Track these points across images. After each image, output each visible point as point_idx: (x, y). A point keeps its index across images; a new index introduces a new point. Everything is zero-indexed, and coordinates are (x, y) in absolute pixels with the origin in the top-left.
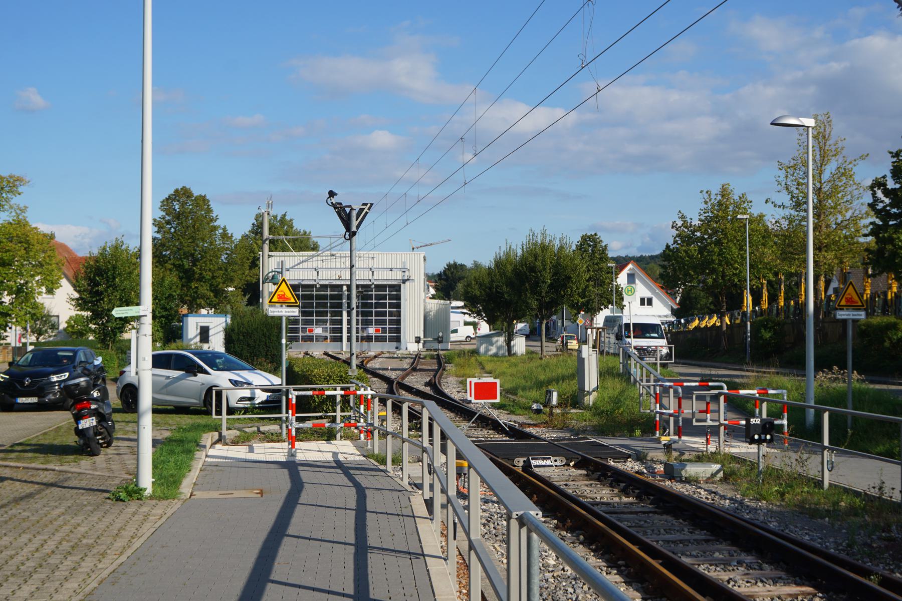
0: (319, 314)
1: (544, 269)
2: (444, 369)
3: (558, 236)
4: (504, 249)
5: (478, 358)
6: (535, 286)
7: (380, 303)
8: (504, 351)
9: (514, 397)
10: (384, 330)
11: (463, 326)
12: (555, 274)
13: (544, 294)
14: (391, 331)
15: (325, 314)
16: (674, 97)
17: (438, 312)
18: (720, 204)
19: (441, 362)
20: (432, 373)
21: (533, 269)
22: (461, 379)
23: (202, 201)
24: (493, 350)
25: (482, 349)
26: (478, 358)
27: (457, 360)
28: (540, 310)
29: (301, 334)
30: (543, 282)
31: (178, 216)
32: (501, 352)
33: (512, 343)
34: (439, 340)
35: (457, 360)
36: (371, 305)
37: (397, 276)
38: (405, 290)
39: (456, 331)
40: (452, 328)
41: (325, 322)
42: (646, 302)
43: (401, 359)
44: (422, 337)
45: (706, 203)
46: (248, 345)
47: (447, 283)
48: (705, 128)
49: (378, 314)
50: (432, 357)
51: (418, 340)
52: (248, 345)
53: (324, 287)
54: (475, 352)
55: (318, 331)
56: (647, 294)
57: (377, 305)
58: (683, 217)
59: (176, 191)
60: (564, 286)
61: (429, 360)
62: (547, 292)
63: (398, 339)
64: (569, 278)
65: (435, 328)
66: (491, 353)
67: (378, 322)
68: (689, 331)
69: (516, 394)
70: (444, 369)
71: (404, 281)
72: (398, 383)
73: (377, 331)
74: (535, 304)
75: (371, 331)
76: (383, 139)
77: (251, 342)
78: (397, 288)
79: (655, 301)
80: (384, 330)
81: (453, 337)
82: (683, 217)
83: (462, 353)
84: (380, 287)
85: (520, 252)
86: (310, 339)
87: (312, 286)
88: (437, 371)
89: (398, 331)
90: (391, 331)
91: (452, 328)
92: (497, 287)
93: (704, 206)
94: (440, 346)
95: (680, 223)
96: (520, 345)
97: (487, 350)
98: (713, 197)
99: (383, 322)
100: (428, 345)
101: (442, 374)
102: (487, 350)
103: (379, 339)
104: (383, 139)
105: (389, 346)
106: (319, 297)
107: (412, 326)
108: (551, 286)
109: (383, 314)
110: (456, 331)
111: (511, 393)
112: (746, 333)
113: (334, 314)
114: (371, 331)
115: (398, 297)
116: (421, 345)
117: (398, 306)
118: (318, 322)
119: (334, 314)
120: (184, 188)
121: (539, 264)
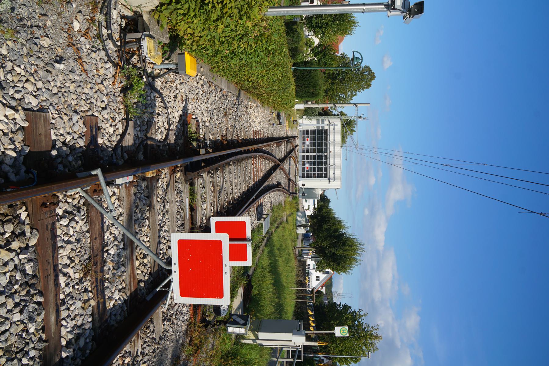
0: (315, 143)
1: (344, 251)
2: (289, 195)
3: (361, 258)
4: (346, 224)
5: (295, 212)
6: (333, 245)
7: (319, 167)
8: (299, 224)
9: (264, 243)
10: (307, 171)
11: (309, 206)
12: (341, 256)
13: (329, 249)
14: (307, 174)
15: (315, 146)
16: (389, 285)
17: (315, 194)
18: (371, 335)
19: (294, 194)
20: (287, 188)
21: (344, 244)
22: (283, 204)
23: (369, 86)
24: (299, 219)
25: (300, 214)
26: (295, 212)
27: (294, 202)
28: (321, 247)
29: (306, 136)
30: (337, 250)
31: (362, 73)
32: (298, 223)
33: (302, 228)
34: (303, 194)
35: (294, 202)
36: (318, 165)
37: (331, 177)
38: (325, 180)
39: (306, 201)
40: (308, 200)
41: (311, 146)
42: (318, 278)
43: (295, 176)
44: (305, 187)
45: (372, 327)
46: (303, 74)
47: (324, 200)
48: (377, 296)
49: (314, 168)
50: (296, 191)
51: (303, 185)
52: (303, 74)
53: (326, 144)
54: (298, 210)
55: (307, 143)
56: (321, 279)
57: (318, 168)
58: (365, 315)
59: (374, 73)
60: (334, 261)
61: (294, 189)
62: (331, 251)
63: (304, 177)
64: (339, 264)
65: (308, 193)
66: (298, 218)
67: (311, 168)
68: (307, 310)
69: (266, 245)
70: (289, 195)
71: (329, 179)
72: (279, 165)
73: (307, 168)
74: (324, 244)
75: (307, 165)
76: (372, 181)
77: (305, 75)
78: (326, 176)
79: (318, 282)
80: (307, 171)
81: (304, 200)
82: (365, 315)
83: (297, 204)
84: (326, 169)
85: (344, 231)
86: (304, 139)
87: (326, 140)
88: (289, 191)
89: (307, 177)
90: (307, 174)
91: (308, 200)
92: (329, 221)
93: (371, 326)
94: (301, 195)
95: (362, 313)
96: (301, 231)
97: (299, 216)
98: (375, 331)
99: (311, 171)
100: (301, 190)
101: (286, 193)
102: (299, 216)
103: (304, 169)
104: (372, 181)
105: (300, 173)
106: (322, 143)
107: (309, 183)
108: (334, 254)
109: (315, 171)
110: (306, 201)
111: (268, 240)
112: (307, 354)
113: (315, 150)
114: (307, 165)
115: (322, 177)
116: (301, 186)
117: (318, 177)
118: (311, 143)
119: (315, 150)
120: (375, 77)
121: (347, 248)
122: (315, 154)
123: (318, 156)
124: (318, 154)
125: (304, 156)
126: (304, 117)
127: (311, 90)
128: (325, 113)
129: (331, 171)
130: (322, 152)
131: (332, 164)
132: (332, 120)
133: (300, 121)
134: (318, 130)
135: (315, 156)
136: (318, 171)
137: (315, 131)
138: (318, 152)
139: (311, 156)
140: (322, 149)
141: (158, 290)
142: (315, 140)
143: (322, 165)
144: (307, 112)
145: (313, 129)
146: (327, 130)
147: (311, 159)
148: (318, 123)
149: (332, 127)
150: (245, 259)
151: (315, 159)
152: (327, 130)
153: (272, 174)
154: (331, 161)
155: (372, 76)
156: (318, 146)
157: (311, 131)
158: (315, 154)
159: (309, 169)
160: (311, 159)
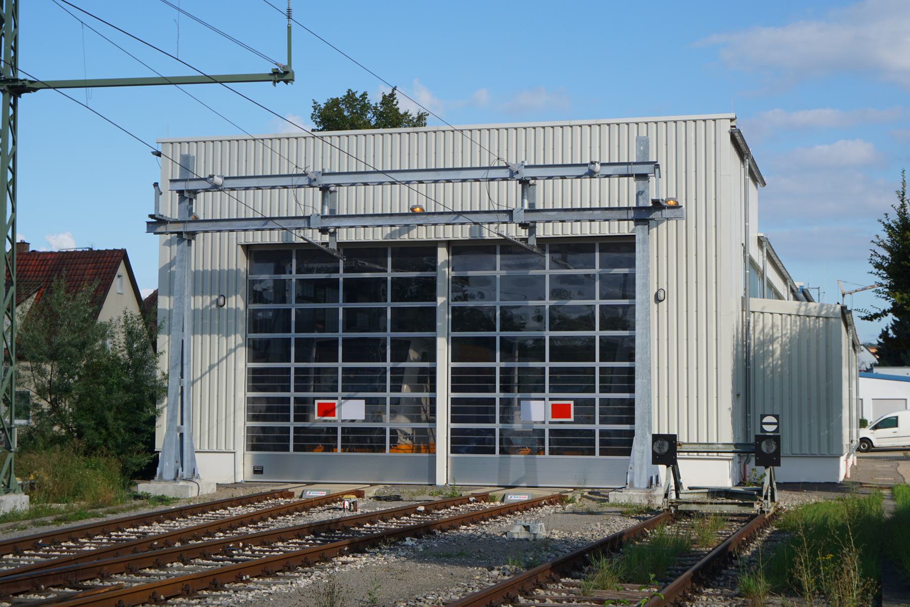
0: (354, 350)
38: (658, 258)
49: (561, 351)
53: (358, 253)
67: (563, 381)
71: (645, 214)
73: (559, 411)
78: (622, 248)
114: (538, 411)
118: (356, 383)
122: (443, 348)
123: (460, 319)
124: (443, 319)
125: (459, 442)
130: (428, 289)
134: (256, 323)
135: (459, 350)
137: (258, 351)
138: (428, 319)
139: (459, 380)
140: (401, 289)
142: (327, 350)
145: (240, 364)
146: (252, 252)
150: (570, 405)
151: (485, 348)
152: (252, 252)
153: (814, 490)
156: (374, 320)
157: (257, 380)
158: (443, 348)
159: (569, 399)
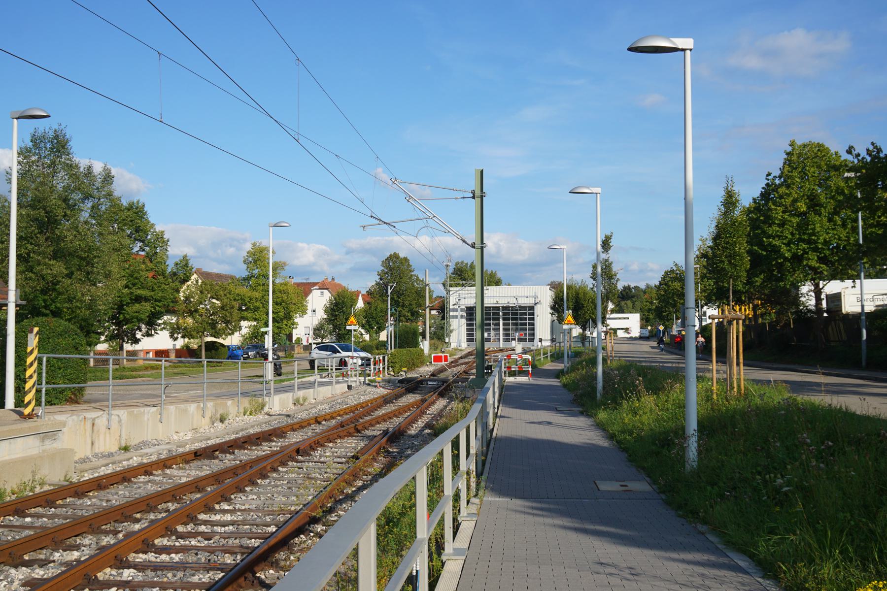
38: (538, 310)
63: (533, 340)
71: (536, 304)
78: (532, 308)
80: (525, 335)
109: (525, 324)
126: (447, 340)
127: (411, 335)
128: (442, 308)
129: (529, 302)
131: (514, 301)
132: (453, 300)
133: (453, 345)
136: (525, 319)
139: (504, 325)
141: (865, 337)
143: (513, 324)
144: (440, 335)
147: (508, 330)
148: (456, 317)
149: (462, 301)
151: (508, 319)
154: (512, 302)
155: (394, 257)
158: (501, 322)
159: (522, 333)
160: (508, 330)
